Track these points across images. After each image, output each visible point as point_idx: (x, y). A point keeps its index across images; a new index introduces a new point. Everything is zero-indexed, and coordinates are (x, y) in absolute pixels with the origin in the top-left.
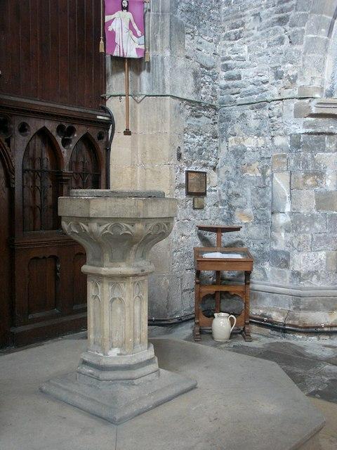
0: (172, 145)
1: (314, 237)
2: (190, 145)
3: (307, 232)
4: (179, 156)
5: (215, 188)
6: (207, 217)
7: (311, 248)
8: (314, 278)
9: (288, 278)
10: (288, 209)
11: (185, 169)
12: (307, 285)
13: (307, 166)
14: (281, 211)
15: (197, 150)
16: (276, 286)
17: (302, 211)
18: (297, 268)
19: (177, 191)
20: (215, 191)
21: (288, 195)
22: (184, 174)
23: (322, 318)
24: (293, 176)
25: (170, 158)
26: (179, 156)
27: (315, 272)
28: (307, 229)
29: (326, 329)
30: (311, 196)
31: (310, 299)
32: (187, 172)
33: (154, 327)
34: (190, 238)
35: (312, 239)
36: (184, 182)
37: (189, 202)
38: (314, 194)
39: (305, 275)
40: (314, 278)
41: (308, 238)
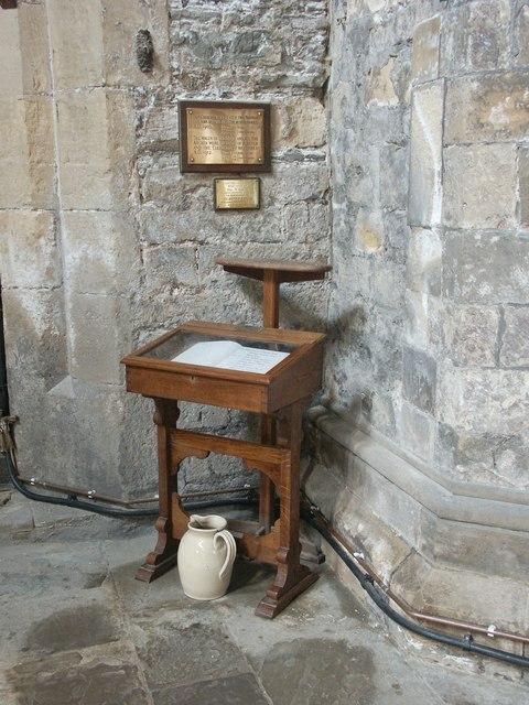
0: (112, 23)
1: (509, 317)
2: (195, 25)
3: (485, 301)
4: (148, 60)
5: (318, 152)
6: (283, 236)
7: (497, 356)
8: (507, 460)
9: (431, 444)
10: (436, 218)
11: (182, 97)
12: (480, 480)
13: (494, 54)
14: (424, 224)
15: (230, 37)
16: (408, 460)
17: (466, 225)
18: (451, 421)
19: (147, 160)
20: (317, 158)
21: (437, 167)
22: (175, 112)
23: (493, 601)
24: (449, 96)
25: (111, 64)
26: (148, 60)
27: (509, 442)
28: (485, 289)
29: (507, 646)
30: (501, 170)
31: (469, 532)
32: (184, 106)
33: (90, 513)
34: (207, 292)
35: (502, 324)
36: (174, 134)
37: (201, 191)
38: (515, 165)
39: (471, 445)
40: (507, 460)
41: (485, 318)
